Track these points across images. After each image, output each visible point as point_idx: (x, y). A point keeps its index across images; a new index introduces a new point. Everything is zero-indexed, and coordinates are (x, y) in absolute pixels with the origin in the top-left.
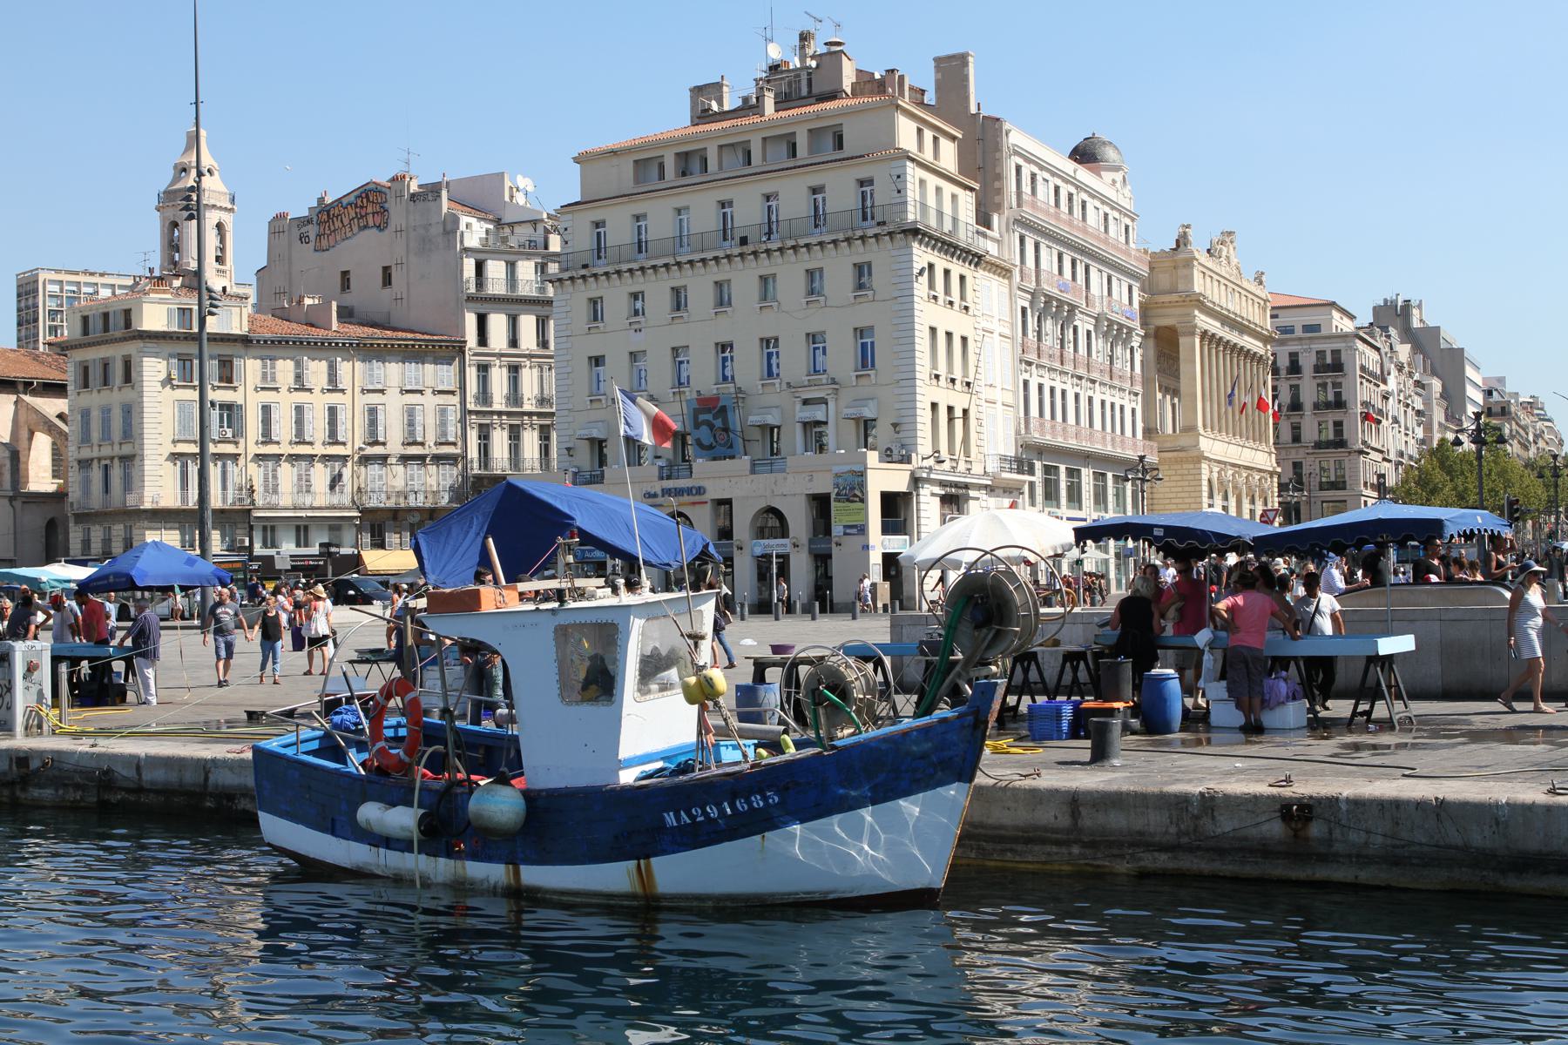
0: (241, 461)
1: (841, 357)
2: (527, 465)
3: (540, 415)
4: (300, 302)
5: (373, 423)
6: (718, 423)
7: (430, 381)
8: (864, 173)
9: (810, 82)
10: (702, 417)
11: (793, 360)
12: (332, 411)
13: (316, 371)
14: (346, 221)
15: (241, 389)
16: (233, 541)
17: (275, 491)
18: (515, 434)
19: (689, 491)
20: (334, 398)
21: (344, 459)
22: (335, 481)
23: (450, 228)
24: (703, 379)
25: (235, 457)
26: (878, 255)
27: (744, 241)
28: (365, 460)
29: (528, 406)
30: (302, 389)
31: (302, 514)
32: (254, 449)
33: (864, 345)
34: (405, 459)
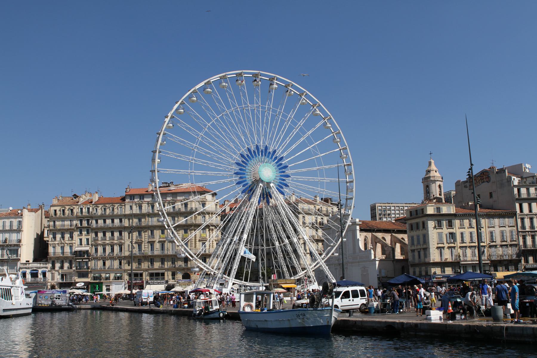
0: (456, 248)
4: (468, 203)
5: (492, 236)
7: (507, 224)
17: (466, 256)
25: (454, 247)
28: (490, 247)
32: (459, 245)
34: (502, 246)
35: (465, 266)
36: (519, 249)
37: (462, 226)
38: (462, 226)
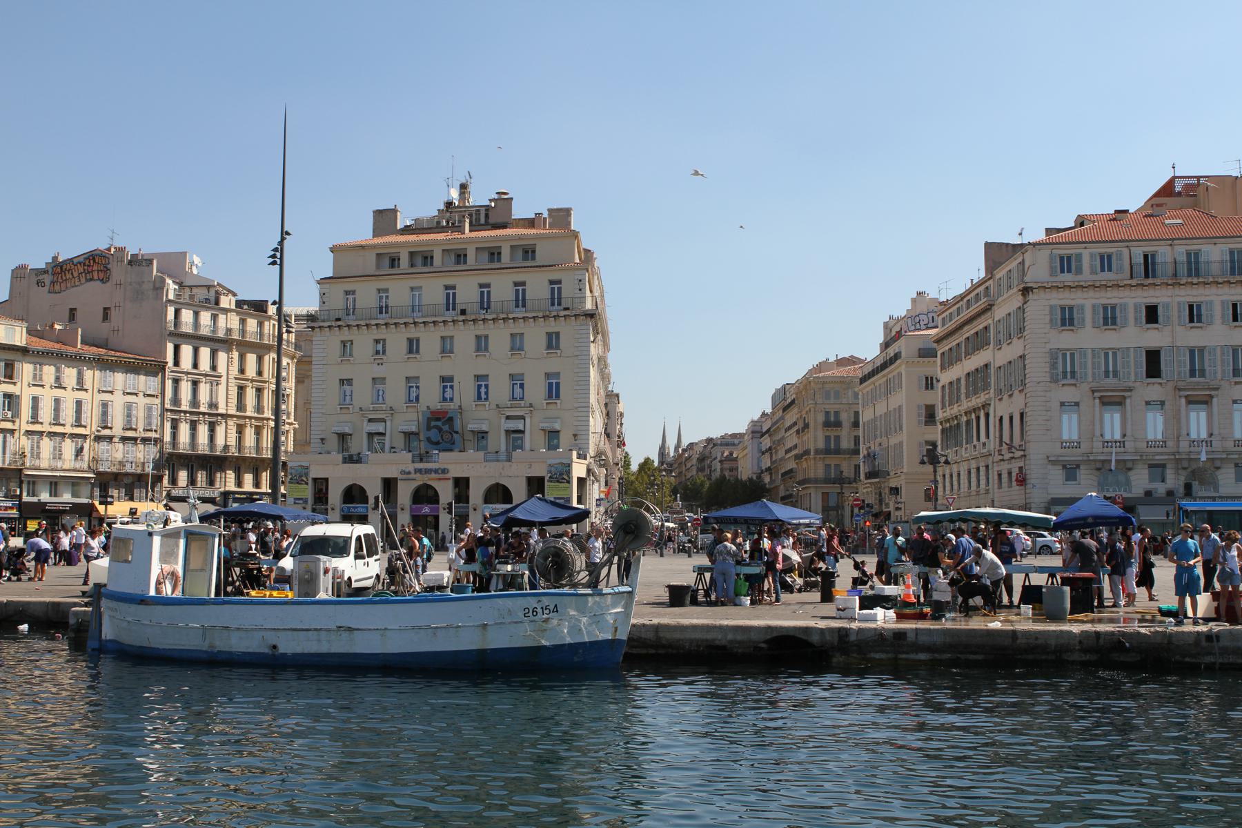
0: (17, 434)
1: (536, 390)
2: (200, 447)
3: (210, 415)
4: (52, 326)
5: (105, 413)
6: (446, 428)
7: (142, 388)
8: (555, 276)
9: (487, 216)
10: (433, 423)
11: (500, 390)
12: (79, 404)
13: (70, 374)
14: (75, 274)
15: (19, 384)
16: (8, 490)
17: (38, 457)
18: (194, 427)
19: (436, 471)
20: (80, 395)
21: (84, 437)
22: (79, 452)
23: (159, 287)
24: (431, 398)
25: (12, 432)
26: (566, 329)
27: (463, 312)
28: (99, 439)
29: (203, 409)
30: (60, 387)
31: (58, 474)
32: (25, 427)
33: (550, 385)
34: (124, 439)
35: (33, 482)
36: (161, 452)
37: (37, 383)
38: (37, 383)
